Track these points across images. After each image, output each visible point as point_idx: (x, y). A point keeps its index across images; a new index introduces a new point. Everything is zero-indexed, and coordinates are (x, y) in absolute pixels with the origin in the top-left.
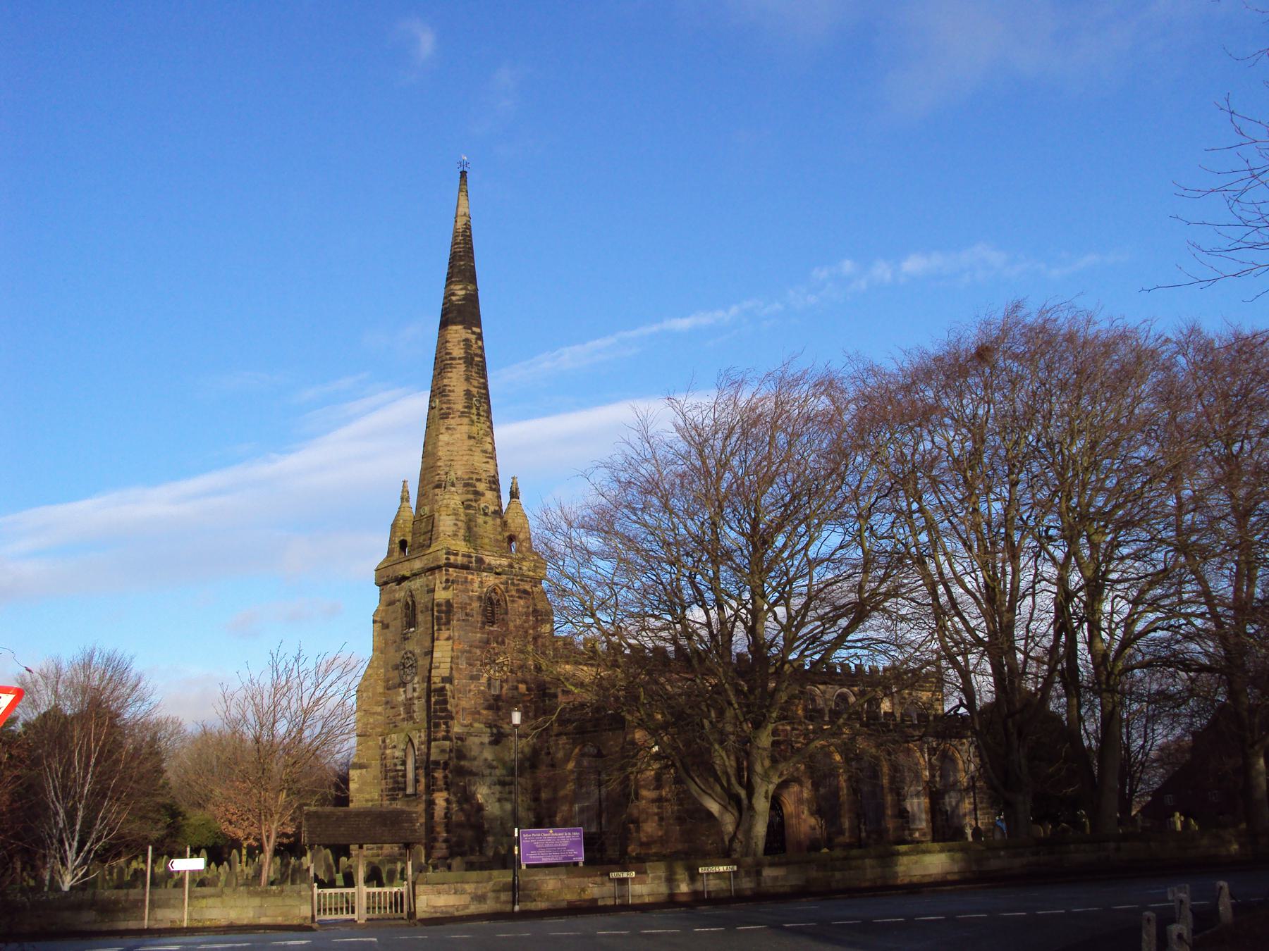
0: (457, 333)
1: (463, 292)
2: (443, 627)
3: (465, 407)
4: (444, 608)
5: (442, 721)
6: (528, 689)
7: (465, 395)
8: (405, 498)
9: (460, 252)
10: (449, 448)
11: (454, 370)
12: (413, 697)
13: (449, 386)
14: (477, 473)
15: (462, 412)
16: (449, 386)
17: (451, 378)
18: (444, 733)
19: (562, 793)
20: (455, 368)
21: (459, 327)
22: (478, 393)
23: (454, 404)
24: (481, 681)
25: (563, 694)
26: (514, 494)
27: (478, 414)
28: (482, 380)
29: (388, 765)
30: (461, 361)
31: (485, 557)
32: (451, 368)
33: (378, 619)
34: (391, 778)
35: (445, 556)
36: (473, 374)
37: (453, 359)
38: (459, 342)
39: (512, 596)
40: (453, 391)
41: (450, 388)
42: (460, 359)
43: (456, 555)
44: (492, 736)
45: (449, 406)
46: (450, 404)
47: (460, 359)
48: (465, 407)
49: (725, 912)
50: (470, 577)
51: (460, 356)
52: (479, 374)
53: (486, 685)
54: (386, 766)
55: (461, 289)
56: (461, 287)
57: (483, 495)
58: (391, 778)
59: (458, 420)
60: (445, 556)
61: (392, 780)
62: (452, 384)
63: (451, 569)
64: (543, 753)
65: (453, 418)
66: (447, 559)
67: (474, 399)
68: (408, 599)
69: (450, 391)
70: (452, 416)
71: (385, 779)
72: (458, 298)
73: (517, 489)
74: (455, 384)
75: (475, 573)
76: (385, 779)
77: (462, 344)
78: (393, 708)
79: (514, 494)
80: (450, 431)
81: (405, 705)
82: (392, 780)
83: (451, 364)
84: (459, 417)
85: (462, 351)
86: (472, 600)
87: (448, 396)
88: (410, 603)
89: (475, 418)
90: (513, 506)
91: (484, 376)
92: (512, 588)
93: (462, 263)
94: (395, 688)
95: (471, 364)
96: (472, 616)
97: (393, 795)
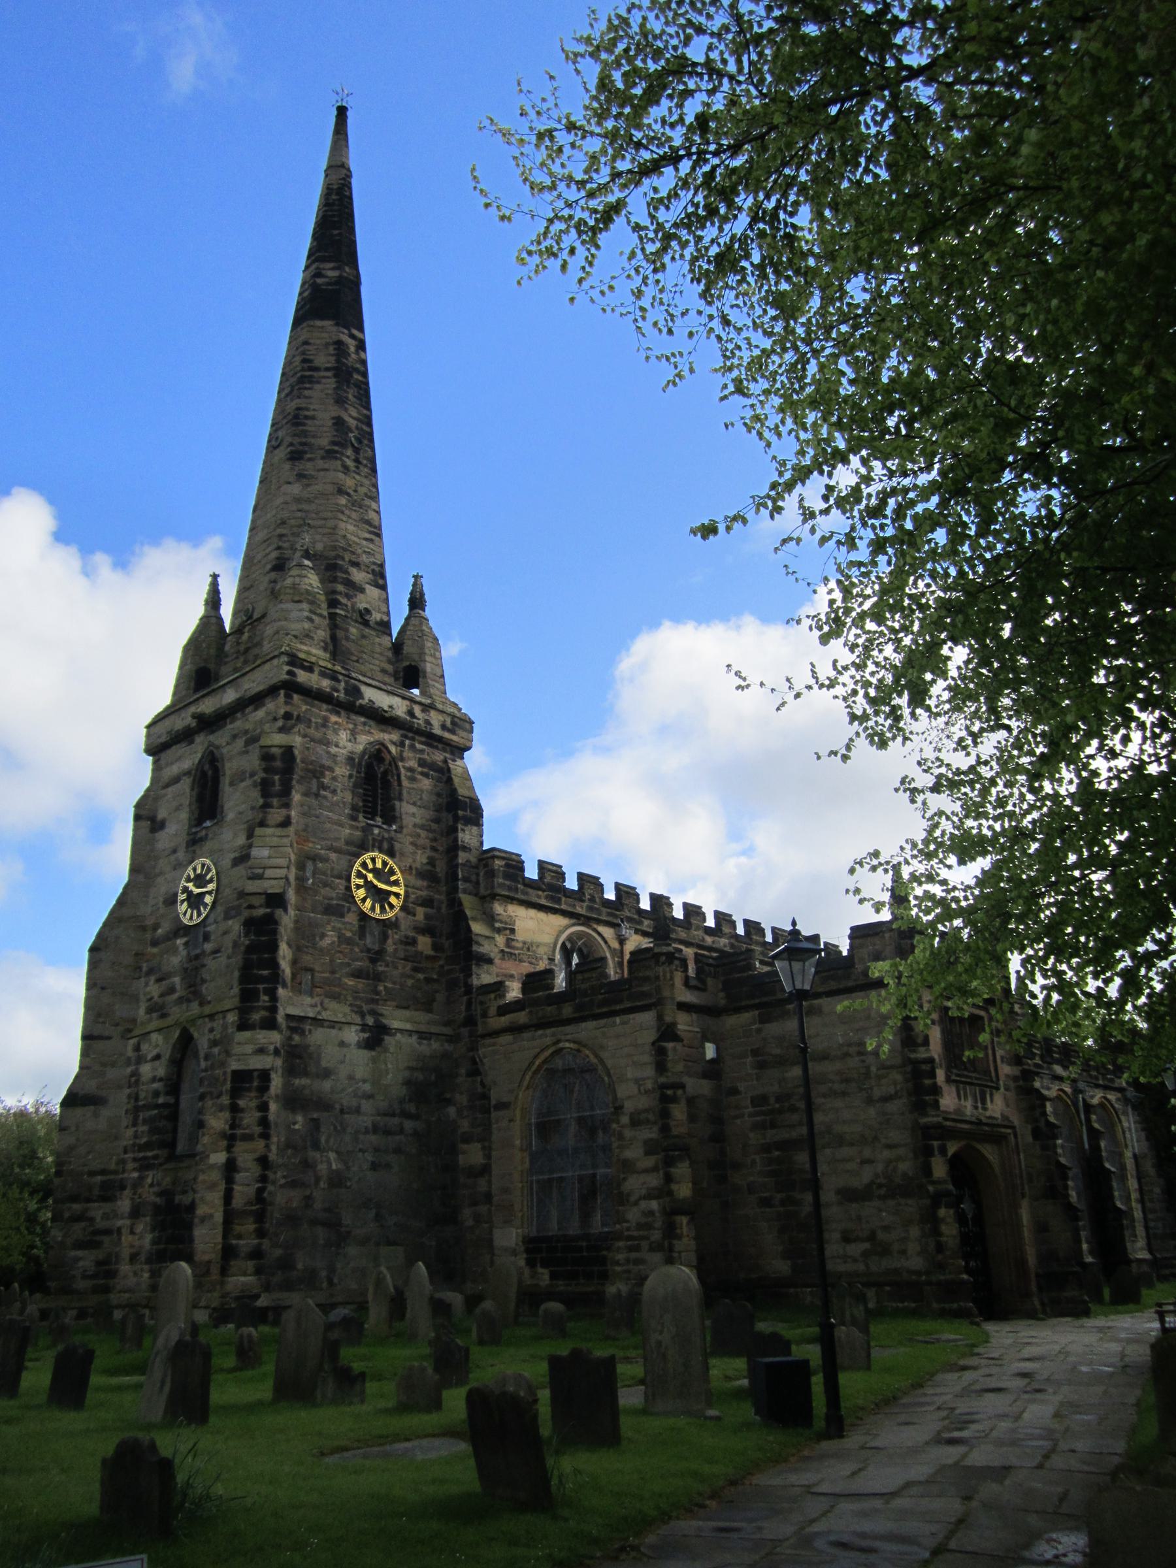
0: (326, 330)
1: (335, 274)
2: (275, 801)
3: (334, 443)
4: (278, 764)
5: (261, 987)
6: (436, 947)
7: (334, 424)
8: (214, 600)
9: (334, 216)
10: (300, 507)
11: (317, 386)
12: (203, 952)
13: (307, 409)
14: (353, 553)
15: (329, 452)
16: (307, 409)
17: (310, 397)
18: (263, 1013)
19: (825, 426)
20: (319, 382)
21: (327, 323)
22: (357, 428)
23: (314, 437)
24: (346, 919)
25: (503, 959)
26: (417, 602)
27: (357, 461)
28: (365, 412)
29: (142, 1095)
30: (329, 374)
31: (363, 688)
32: (311, 382)
33: (143, 813)
34: (145, 1121)
35: (286, 668)
36: (350, 396)
37: (317, 369)
38: (327, 345)
39: (411, 770)
40: (313, 418)
41: (307, 413)
42: (327, 369)
43: (310, 669)
44: (363, 1031)
45: (304, 440)
46: (306, 437)
47: (327, 369)
48: (334, 443)
49: (1025, 1222)
50: (334, 718)
51: (329, 365)
52: (360, 399)
53: (356, 928)
54: (137, 1099)
55: (333, 269)
56: (331, 265)
57: (362, 591)
58: (145, 1121)
59: (320, 463)
60: (286, 668)
61: (145, 1128)
62: (312, 407)
63: (295, 696)
64: (463, 1071)
65: (310, 460)
66: (290, 673)
67: (351, 435)
68: (207, 767)
69: (306, 417)
70: (308, 456)
71: (135, 1124)
72: (326, 280)
73: (422, 594)
74: (316, 407)
75: (343, 713)
76: (135, 1124)
77: (331, 348)
78: (159, 980)
79: (417, 602)
80: (305, 481)
81: (186, 970)
82: (145, 1128)
83: (311, 376)
84: (323, 458)
85: (333, 359)
86: (335, 762)
87: (304, 425)
88: (210, 773)
89: (350, 463)
90: (413, 621)
91: (367, 405)
92: (411, 755)
93: (336, 232)
94: (169, 939)
95: (348, 383)
96: (334, 792)
97: (145, 1158)
